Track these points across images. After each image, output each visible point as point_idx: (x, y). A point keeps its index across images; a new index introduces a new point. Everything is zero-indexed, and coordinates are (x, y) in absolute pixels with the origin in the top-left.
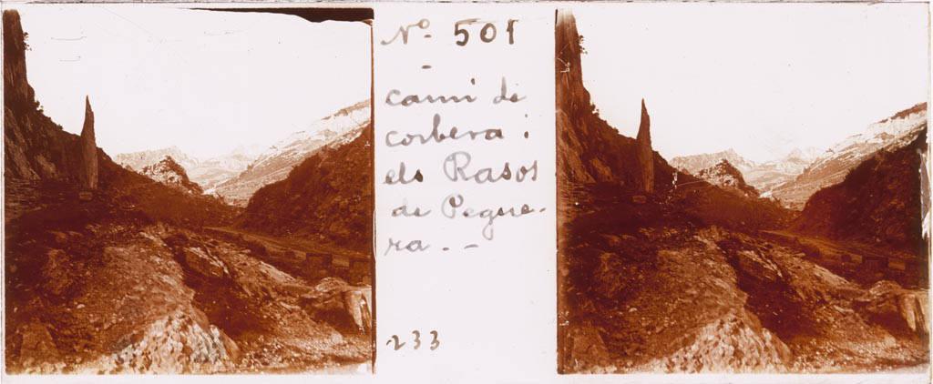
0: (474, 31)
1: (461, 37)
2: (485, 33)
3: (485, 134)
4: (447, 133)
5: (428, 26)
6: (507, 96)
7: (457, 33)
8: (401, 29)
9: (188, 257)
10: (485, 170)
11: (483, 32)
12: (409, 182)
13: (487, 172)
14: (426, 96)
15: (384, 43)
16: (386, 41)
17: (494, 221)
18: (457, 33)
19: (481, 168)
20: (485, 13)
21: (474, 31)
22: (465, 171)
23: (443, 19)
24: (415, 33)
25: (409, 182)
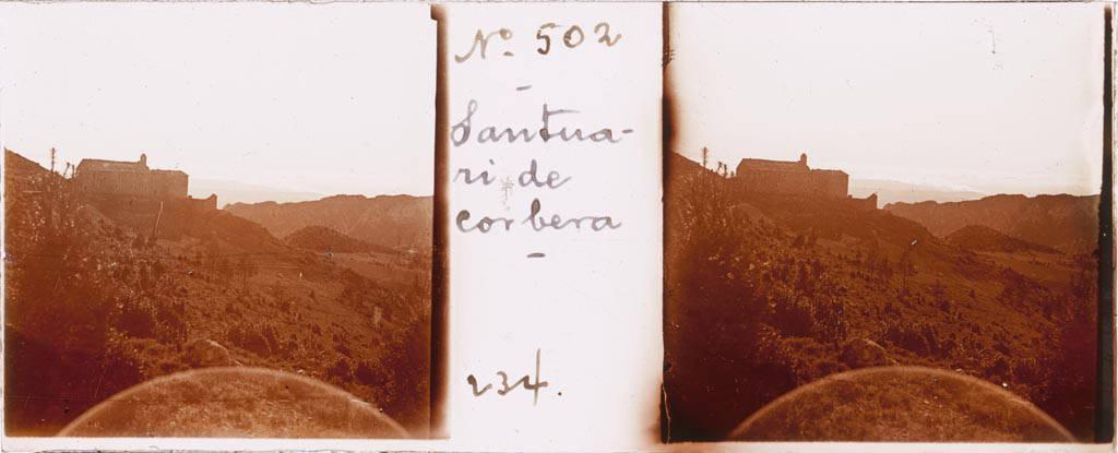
0: (556, 36)
1: (542, 44)
2: (569, 38)
3: (522, 384)
4: (548, 221)
5: (510, 37)
6: (546, 222)
7: (539, 37)
8: (479, 36)
9: (679, 160)
10: (481, 393)
11: (568, 36)
12: (500, 219)
13: (479, 391)
14: (505, 128)
15: (458, 59)
16: (461, 55)
17: (466, 116)
18: (539, 37)
19: (583, 30)
20: (565, 16)
21: (556, 36)
22: (529, 170)
23: (525, 21)
24: (496, 44)
25: (500, 219)
